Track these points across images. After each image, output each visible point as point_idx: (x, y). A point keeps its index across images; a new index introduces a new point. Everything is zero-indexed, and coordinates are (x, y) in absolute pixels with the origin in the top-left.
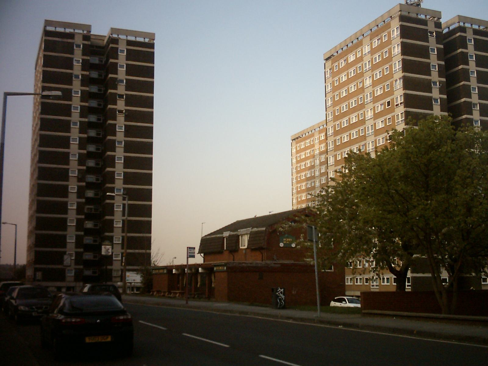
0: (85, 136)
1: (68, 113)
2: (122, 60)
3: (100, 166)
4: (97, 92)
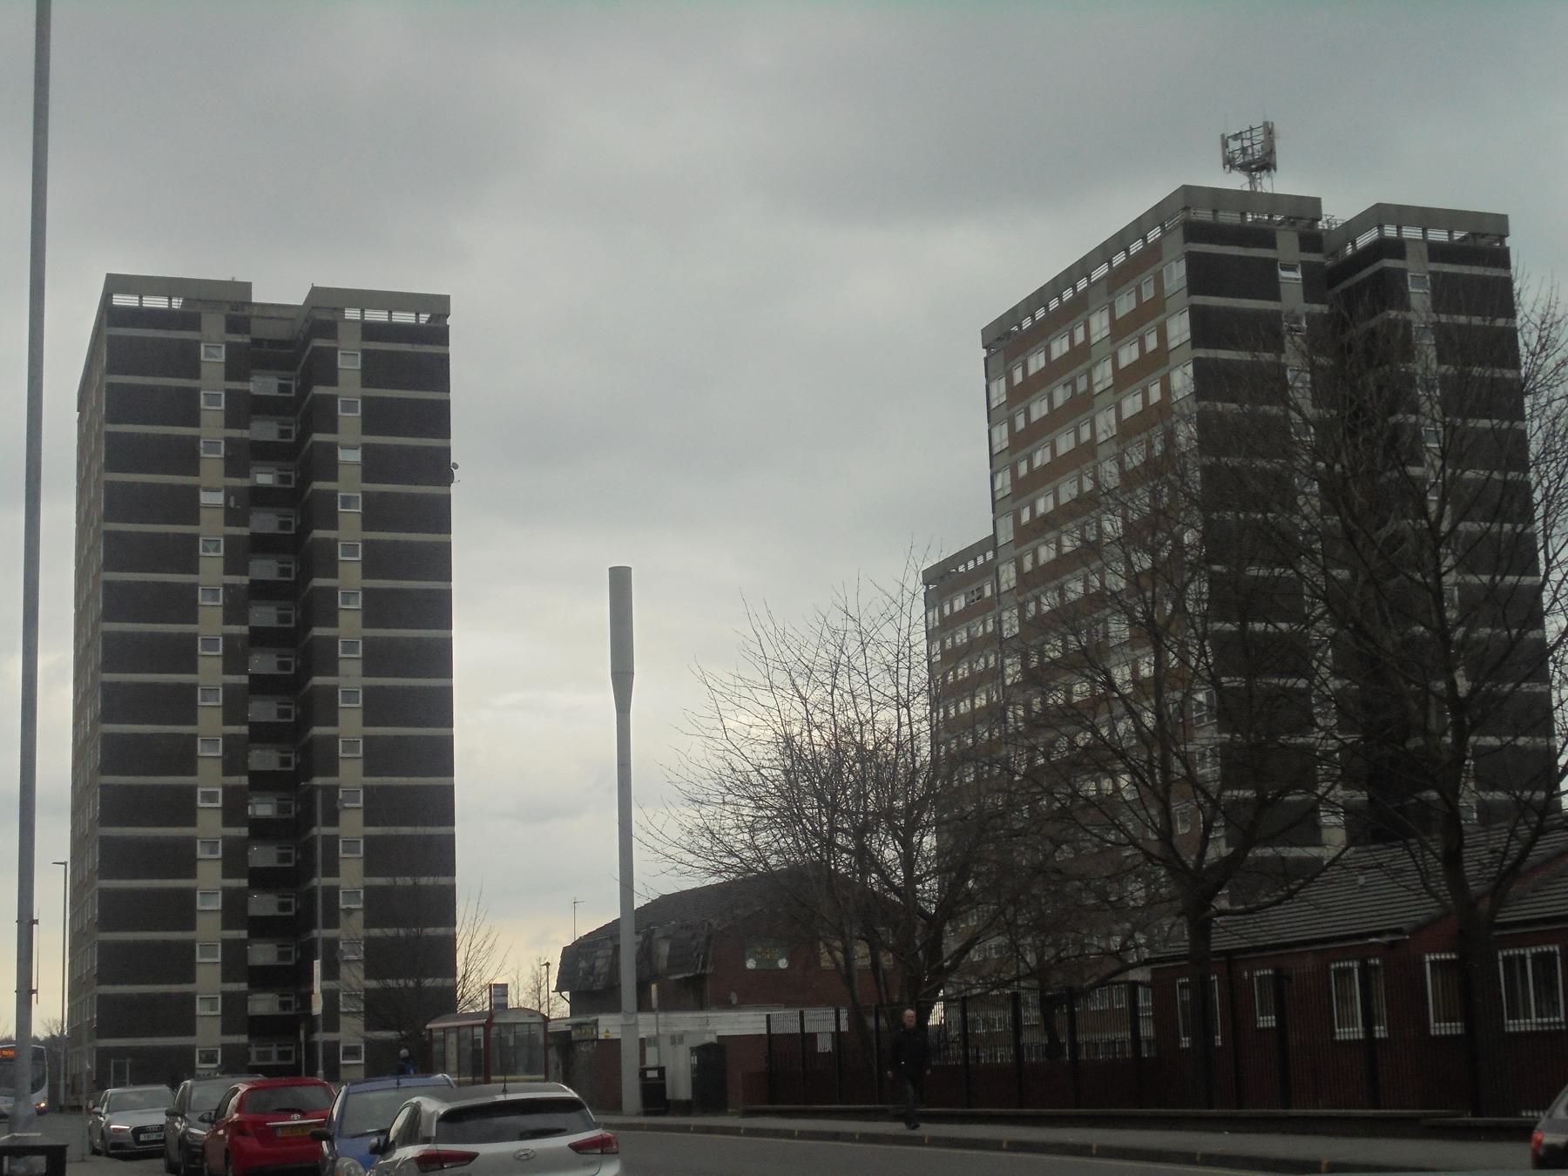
0: (245, 531)
1: (189, 612)
2: (349, 364)
3: (292, 625)
4: (278, 672)
